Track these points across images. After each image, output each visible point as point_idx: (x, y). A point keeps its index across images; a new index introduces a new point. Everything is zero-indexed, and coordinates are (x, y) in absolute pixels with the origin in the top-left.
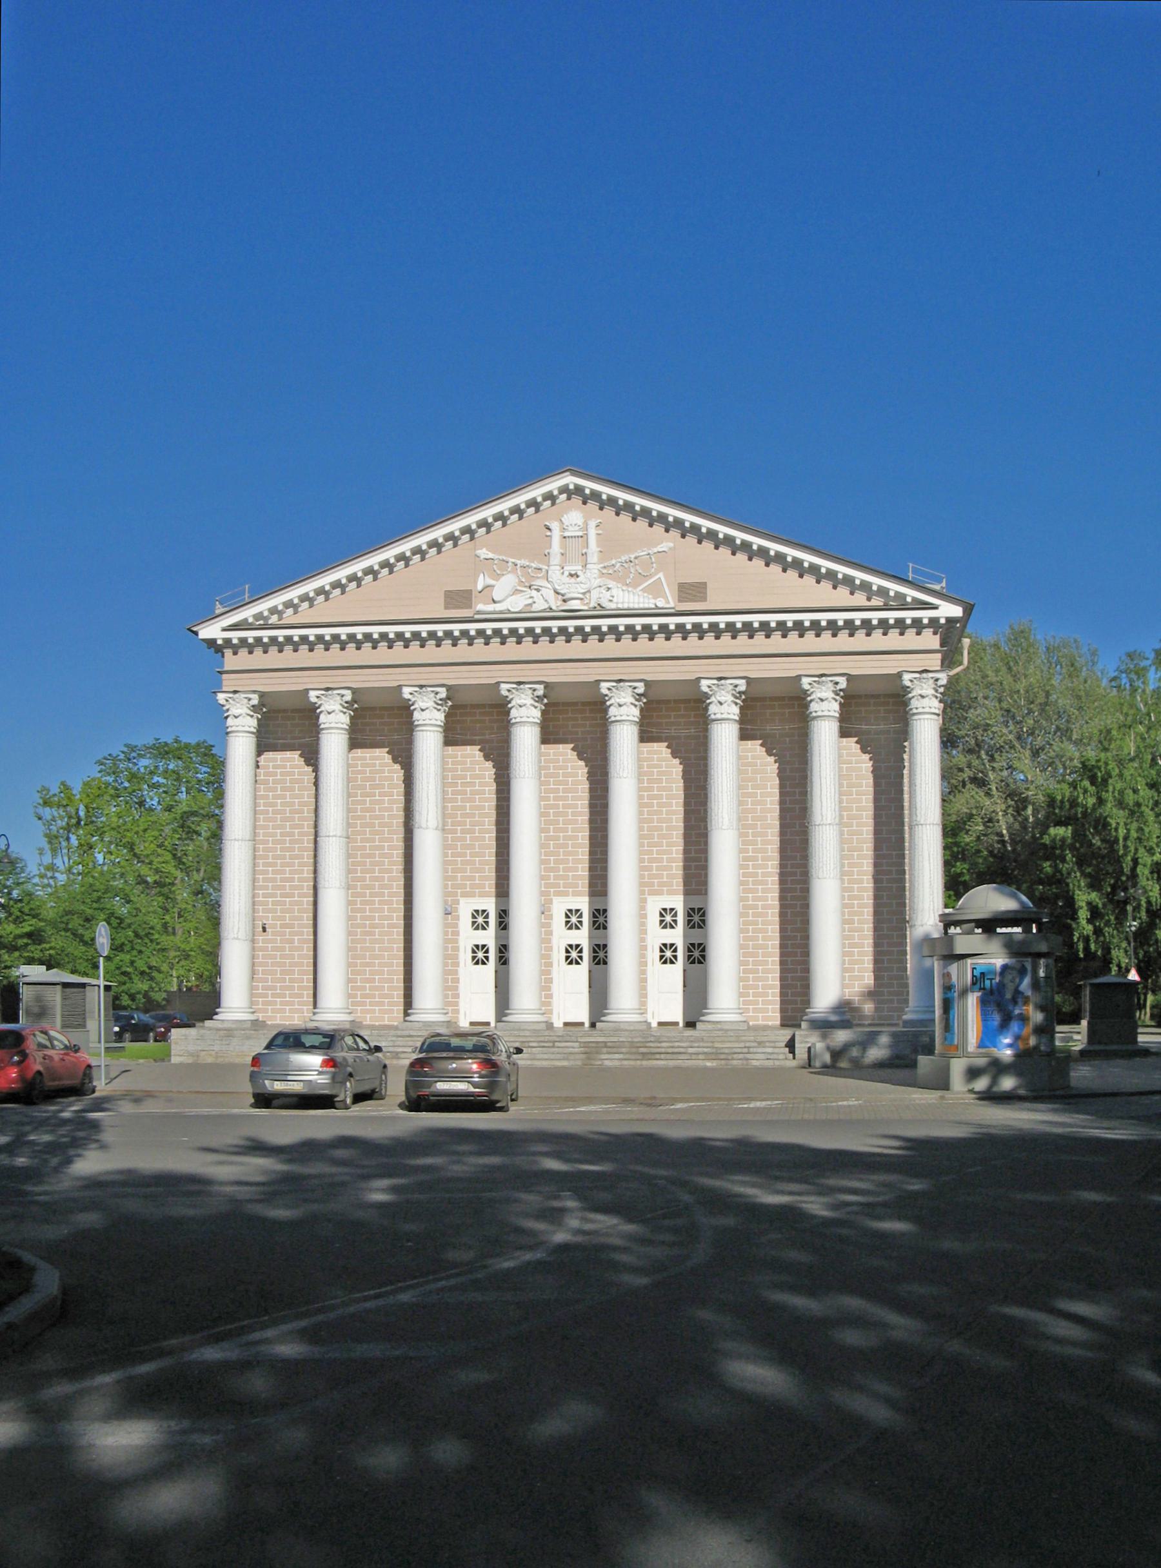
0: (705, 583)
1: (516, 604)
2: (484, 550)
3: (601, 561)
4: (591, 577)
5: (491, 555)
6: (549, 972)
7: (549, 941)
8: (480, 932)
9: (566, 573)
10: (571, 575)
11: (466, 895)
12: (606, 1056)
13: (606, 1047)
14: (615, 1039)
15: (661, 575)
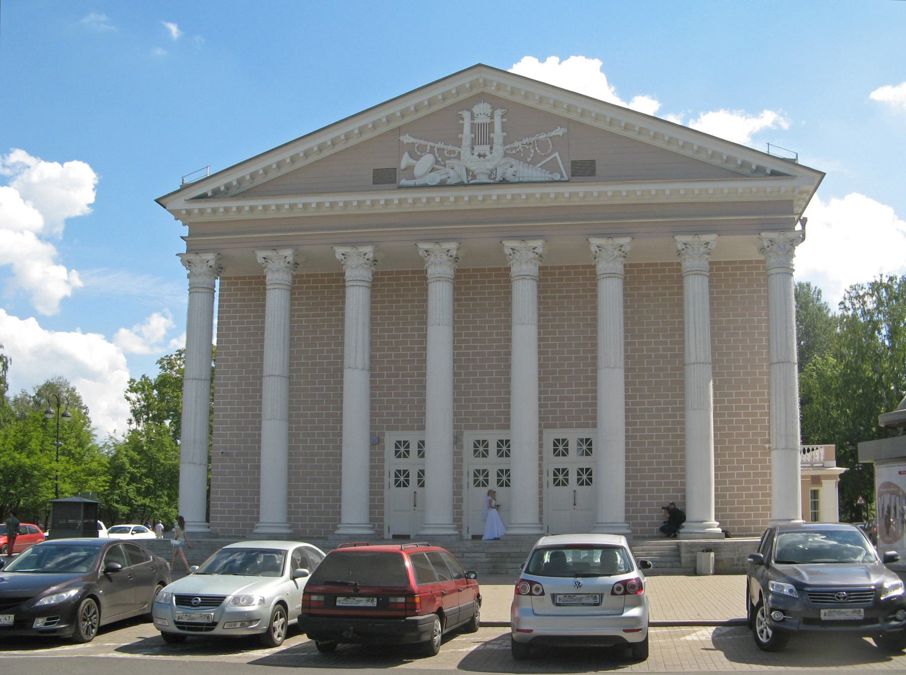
0: (593, 162)
1: (435, 178)
3: (505, 143)
6: (460, 493)
7: (461, 467)
8: (561, 467)
9: (476, 153)
10: (480, 156)
11: (390, 428)
12: (511, 565)
13: (509, 557)
14: (518, 550)
15: (556, 154)
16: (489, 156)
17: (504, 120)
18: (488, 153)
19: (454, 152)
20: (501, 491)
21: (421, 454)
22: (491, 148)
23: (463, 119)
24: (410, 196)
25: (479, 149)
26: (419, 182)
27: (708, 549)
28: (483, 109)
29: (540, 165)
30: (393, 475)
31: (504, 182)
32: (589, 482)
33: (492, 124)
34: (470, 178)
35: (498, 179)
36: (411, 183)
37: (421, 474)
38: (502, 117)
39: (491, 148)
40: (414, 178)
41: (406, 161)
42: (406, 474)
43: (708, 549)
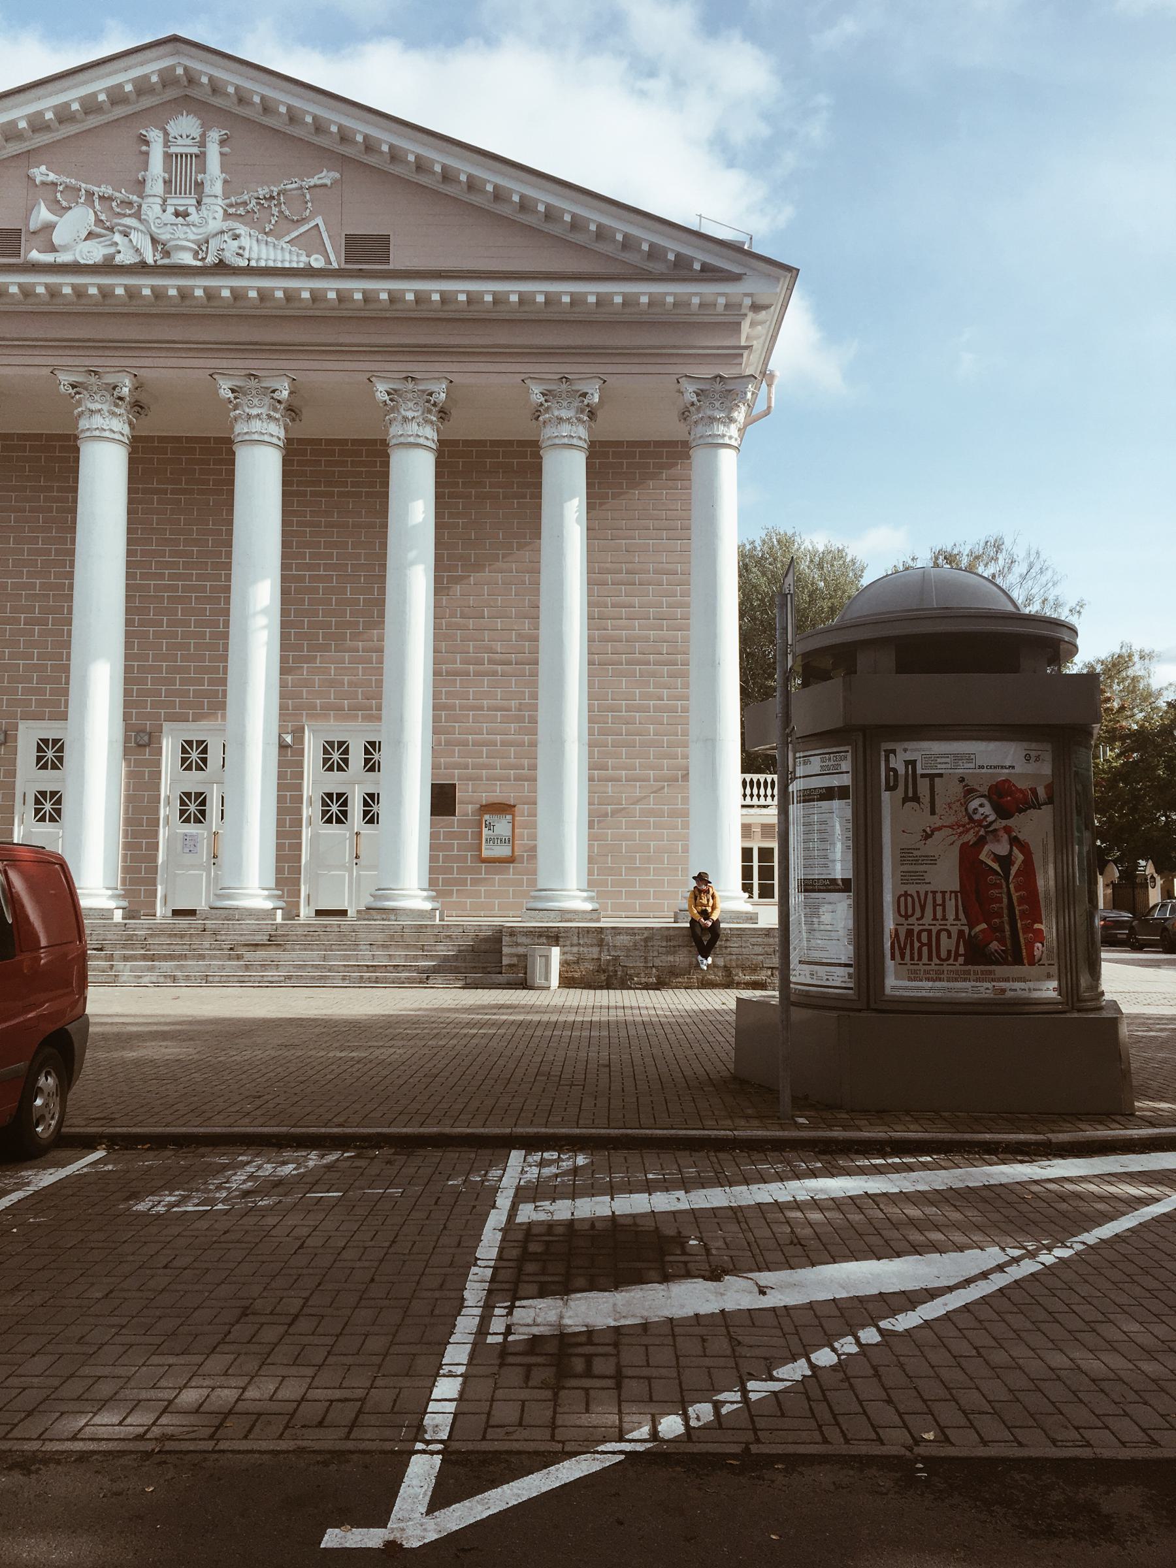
1: (93, 253)
2: (43, 168)
4: (212, 217)
5: (52, 177)
9: (170, 210)
15: (319, 220)
16: (194, 217)
17: (226, 150)
18: (192, 210)
19: (130, 204)
20: (368, 830)
21: (371, 766)
22: (199, 202)
23: (147, 143)
24: (40, 283)
25: (175, 202)
26: (64, 258)
27: (554, 937)
28: (185, 126)
29: (287, 239)
30: (31, 800)
31: (222, 268)
32: (201, 816)
33: (201, 157)
34: (158, 257)
35: (211, 259)
36: (48, 258)
37: (371, 799)
38: (222, 143)
39: (199, 202)
40: (53, 249)
41: (43, 214)
42: (342, 799)
43: (554, 937)
